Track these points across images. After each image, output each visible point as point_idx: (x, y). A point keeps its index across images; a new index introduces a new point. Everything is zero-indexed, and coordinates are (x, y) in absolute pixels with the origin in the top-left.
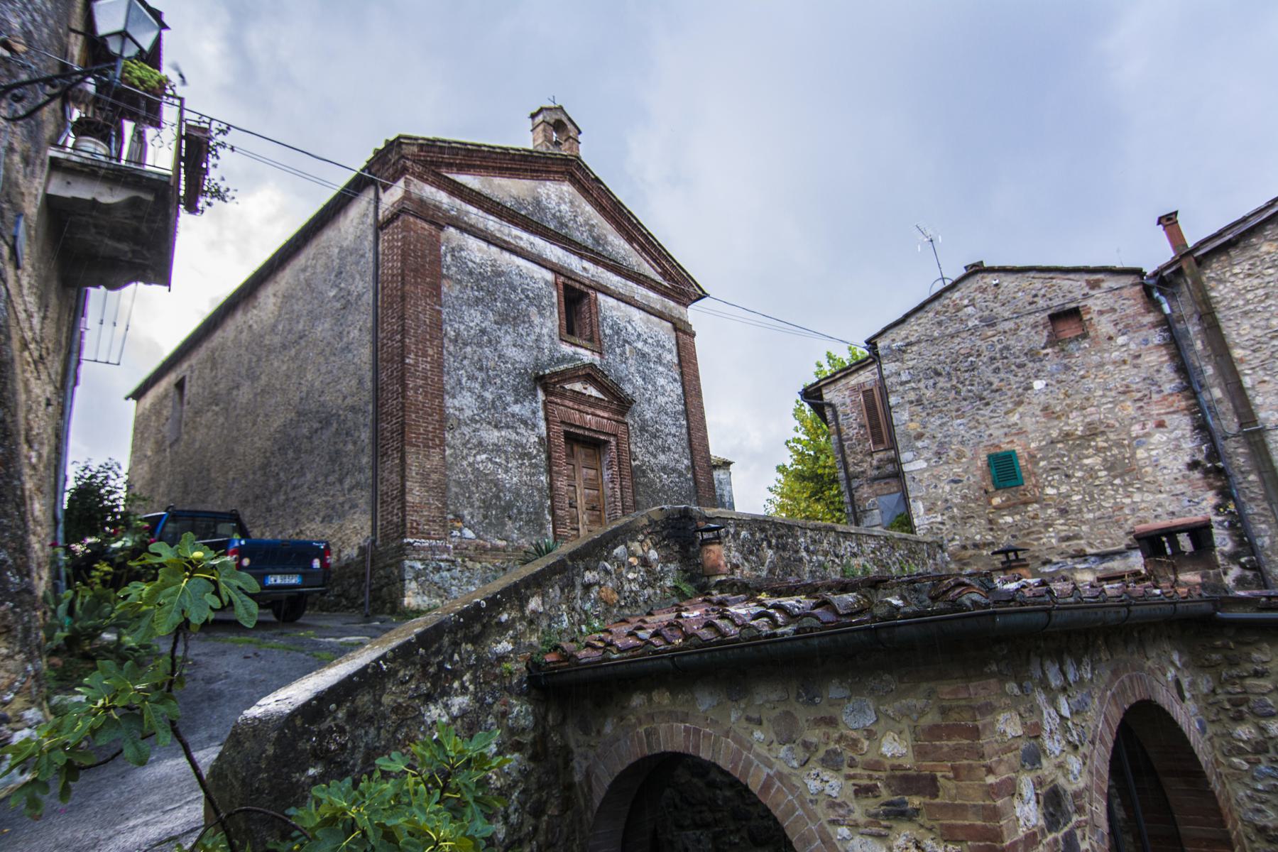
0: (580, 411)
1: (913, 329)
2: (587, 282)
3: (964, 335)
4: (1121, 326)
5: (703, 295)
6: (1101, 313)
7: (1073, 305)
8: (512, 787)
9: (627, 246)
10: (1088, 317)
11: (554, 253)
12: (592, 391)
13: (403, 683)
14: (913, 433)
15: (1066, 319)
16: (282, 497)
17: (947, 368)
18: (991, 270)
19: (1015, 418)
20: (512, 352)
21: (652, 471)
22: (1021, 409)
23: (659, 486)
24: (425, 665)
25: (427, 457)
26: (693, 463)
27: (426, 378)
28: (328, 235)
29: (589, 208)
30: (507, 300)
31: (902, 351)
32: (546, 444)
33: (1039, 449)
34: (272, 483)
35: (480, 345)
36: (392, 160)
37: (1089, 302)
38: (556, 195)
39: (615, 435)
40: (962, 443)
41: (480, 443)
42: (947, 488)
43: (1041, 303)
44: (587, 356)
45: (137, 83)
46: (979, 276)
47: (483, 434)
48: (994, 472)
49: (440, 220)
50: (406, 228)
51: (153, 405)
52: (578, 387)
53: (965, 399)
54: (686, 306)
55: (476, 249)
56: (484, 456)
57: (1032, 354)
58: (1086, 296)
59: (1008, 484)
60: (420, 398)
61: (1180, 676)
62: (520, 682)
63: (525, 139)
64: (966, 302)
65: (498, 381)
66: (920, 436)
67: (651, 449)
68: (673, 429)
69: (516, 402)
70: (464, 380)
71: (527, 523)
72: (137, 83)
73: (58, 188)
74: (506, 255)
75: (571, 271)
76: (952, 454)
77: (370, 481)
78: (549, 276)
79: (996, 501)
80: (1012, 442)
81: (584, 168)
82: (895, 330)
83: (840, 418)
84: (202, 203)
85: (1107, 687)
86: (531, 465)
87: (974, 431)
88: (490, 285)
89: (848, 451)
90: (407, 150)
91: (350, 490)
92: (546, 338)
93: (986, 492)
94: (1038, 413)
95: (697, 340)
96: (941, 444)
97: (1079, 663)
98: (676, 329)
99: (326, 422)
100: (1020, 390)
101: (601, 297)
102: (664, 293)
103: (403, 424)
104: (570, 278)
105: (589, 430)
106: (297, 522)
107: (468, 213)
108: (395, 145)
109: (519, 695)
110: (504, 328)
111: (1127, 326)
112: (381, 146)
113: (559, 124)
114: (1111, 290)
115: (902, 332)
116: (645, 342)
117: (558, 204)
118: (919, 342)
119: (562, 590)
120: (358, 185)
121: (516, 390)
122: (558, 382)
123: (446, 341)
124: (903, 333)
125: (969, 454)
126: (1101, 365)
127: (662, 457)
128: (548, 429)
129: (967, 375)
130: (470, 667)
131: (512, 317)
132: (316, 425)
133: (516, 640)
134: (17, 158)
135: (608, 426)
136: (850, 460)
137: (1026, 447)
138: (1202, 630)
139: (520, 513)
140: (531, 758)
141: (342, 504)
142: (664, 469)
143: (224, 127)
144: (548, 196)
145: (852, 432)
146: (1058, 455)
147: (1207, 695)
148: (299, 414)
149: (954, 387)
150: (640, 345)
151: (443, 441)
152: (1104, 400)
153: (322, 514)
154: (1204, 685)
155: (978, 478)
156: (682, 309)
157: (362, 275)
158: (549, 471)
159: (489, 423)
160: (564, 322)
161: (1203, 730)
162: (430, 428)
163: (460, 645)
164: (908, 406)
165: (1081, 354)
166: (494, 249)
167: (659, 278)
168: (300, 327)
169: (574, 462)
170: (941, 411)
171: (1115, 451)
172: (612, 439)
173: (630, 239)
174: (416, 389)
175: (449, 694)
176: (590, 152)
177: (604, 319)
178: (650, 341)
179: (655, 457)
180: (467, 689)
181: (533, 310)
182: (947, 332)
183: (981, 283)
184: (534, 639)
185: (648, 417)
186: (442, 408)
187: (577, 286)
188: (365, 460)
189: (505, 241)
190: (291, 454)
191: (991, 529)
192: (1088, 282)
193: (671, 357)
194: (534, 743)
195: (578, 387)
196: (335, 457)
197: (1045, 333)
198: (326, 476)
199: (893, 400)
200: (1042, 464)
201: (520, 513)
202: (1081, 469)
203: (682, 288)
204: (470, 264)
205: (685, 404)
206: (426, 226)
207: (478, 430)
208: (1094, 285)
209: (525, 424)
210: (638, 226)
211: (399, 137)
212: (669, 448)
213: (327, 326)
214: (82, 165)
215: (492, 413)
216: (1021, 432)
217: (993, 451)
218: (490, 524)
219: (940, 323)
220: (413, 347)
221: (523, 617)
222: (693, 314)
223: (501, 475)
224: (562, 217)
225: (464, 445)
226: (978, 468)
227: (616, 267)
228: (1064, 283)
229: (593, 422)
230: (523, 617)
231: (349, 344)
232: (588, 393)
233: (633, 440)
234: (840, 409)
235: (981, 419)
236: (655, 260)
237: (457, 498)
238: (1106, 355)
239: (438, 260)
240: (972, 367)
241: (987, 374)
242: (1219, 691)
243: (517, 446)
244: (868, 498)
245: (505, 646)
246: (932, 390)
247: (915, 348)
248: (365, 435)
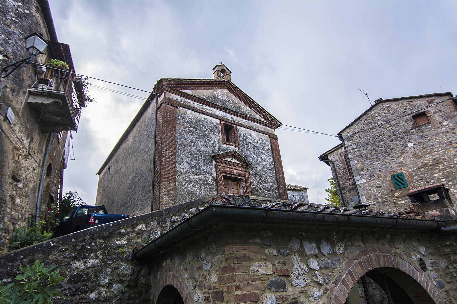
0: (230, 168)
1: (356, 128)
2: (233, 122)
3: (377, 128)
4: (444, 117)
5: (281, 125)
6: (435, 113)
7: (422, 111)
8: (113, 298)
9: (249, 109)
10: (429, 115)
11: (220, 113)
12: (235, 161)
13: (61, 251)
14: (359, 169)
15: (420, 116)
17: (371, 142)
18: (386, 101)
19: (401, 159)
20: (203, 148)
21: (261, 189)
22: (404, 156)
24: (75, 246)
25: (169, 185)
26: (278, 186)
28: (146, 114)
29: (234, 97)
30: (202, 131)
31: (352, 136)
32: (216, 180)
33: (413, 171)
35: (190, 146)
36: (161, 87)
37: (429, 109)
38: (221, 94)
39: (244, 177)
40: (380, 171)
41: (190, 180)
42: (375, 190)
43: (408, 112)
44: (233, 148)
45: (55, 66)
46: (381, 104)
48: (394, 182)
51: (103, 176)
52: (229, 159)
53: (380, 154)
57: (407, 133)
58: (427, 107)
59: (401, 187)
60: (167, 165)
61: (424, 259)
62: (128, 256)
63: (212, 76)
64: (377, 115)
65: (197, 158)
66: (362, 170)
68: (269, 174)
69: (204, 165)
72: (55, 66)
73: (31, 100)
74: (202, 115)
75: (227, 119)
76: (376, 176)
78: (218, 121)
79: (397, 194)
80: (401, 169)
81: (232, 84)
82: (349, 129)
83: (336, 166)
84: (86, 103)
85: (356, 258)
86: (210, 188)
87: (384, 166)
88: (195, 126)
89: (340, 179)
90: (165, 83)
92: (217, 143)
93: (392, 191)
94: (411, 156)
96: (371, 172)
97: (333, 245)
98: (270, 137)
99: (142, 176)
100: (403, 148)
101: (238, 127)
102: (265, 124)
103: (160, 174)
104: (226, 122)
105: (234, 175)
106: (134, 211)
107: (187, 102)
108: (160, 82)
109: (126, 262)
110: (200, 140)
111: (447, 117)
113: (222, 70)
114: (438, 103)
115: (352, 129)
116: (257, 142)
117: (222, 97)
118: (359, 132)
119: (158, 223)
120: (152, 97)
121: (204, 161)
122: (221, 158)
123: (178, 145)
124: (352, 130)
125: (383, 176)
126: (437, 134)
127: (265, 184)
129: (379, 143)
130: (101, 249)
131: (204, 136)
132: (140, 177)
133: (129, 240)
134: (8, 90)
135: (241, 173)
136: (341, 182)
137: (407, 171)
138: (434, 235)
140: (127, 287)
142: (265, 189)
143: (86, 77)
144: (218, 94)
145: (341, 171)
146: (422, 174)
147: (444, 269)
149: (374, 149)
150: (255, 144)
151: (175, 180)
152: (440, 149)
154: (443, 264)
155: (388, 185)
156: (273, 130)
158: (217, 190)
159: (193, 173)
161: (441, 286)
163: (96, 239)
164: (356, 158)
165: (428, 130)
166: (196, 113)
167: (263, 120)
169: (228, 187)
170: (370, 159)
171: (448, 170)
172: (243, 178)
173: (251, 107)
174: (165, 162)
175: (88, 258)
176: (235, 80)
177: (240, 135)
178: (259, 142)
179: (262, 184)
180: (99, 257)
181: (212, 133)
182: (370, 127)
183: (382, 107)
184: (139, 240)
185: (258, 169)
186: (175, 169)
187: (229, 124)
189: (201, 111)
190: (133, 188)
191: (395, 206)
192: (428, 101)
194: (130, 281)
195: (229, 159)
197: (411, 124)
199: (350, 156)
200: (415, 177)
202: (433, 179)
203: (273, 123)
204: (188, 119)
205: (274, 164)
206: (171, 107)
207: (189, 176)
208: (431, 102)
209: (208, 173)
210: (253, 102)
211: (161, 79)
212: (268, 181)
213: (144, 144)
214: (38, 92)
215: (195, 169)
216: (405, 165)
217: (393, 173)
219: (367, 124)
221: (134, 231)
222: (277, 132)
223: (198, 192)
224: (223, 101)
225: (184, 181)
226: (387, 181)
227: (244, 117)
228: (418, 102)
229: (235, 172)
230: (134, 231)
231: (149, 149)
232: (232, 161)
234: (335, 163)
235: (387, 161)
237: (180, 200)
238: (439, 130)
239: (176, 118)
240: (382, 140)
241: (388, 142)
242: (450, 267)
243: (204, 181)
244: (349, 197)
245: (123, 242)
246: (365, 151)
247: (357, 135)
248: (151, 179)
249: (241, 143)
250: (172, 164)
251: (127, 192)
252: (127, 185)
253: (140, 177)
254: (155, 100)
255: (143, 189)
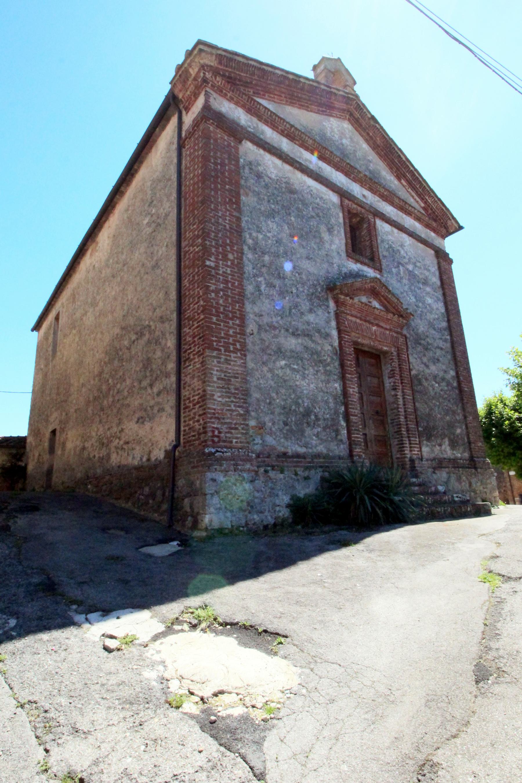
5: (461, 228)
9: (396, 182)
11: (339, 178)
16: (111, 399)
21: (426, 379)
23: (432, 393)
26: (457, 373)
27: (226, 282)
29: (365, 146)
34: (104, 387)
41: (279, 349)
47: (282, 340)
49: (237, 133)
50: (207, 136)
54: (444, 237)
55: (272, 165)
56: (283, 363)
67: (425, 360)
68: (440, 342)
69: (311, 311)
70: (263, 287)
71: (324, 429)
74: (299, 175)
77: (174, 386)
78: (334, 198)
81: (360, 107)
88: (287, 201)
91: (159, 394)
95: (453, 266)
112: (450, 256)
128: (340, 338)
132: (134, 337)
139: (317, 419)
141: (152, 407)
148: (123, 329)
150: (410, 267)
153: (137, 416)
157: (168, 196)
160: (349, 241)
162: (231, 332)
166: (287, 167)
168: (124, 257)
179: (427, 366)
181: (323, 228)
188: (171, 366)
193: (435, 280)
196: (147, 363)
198: (140, 382)
201: (317, 419)
203: (442, 222)
205: (449, 321)
212: (438, 360)
213: (142, 250)
218: (291, 431)
220: (213, 250)
222: (451, 244)
227: (389, 197)
233: (410, 351)
236: (419, 195)
243: (312, 354)
248: (171, 343)
249: (384, 262)
250: (234, 302)
251: (100, 374)
252: (100, 355)
253: (134, 337)
254: (174, 121)
255: (145, 367)
